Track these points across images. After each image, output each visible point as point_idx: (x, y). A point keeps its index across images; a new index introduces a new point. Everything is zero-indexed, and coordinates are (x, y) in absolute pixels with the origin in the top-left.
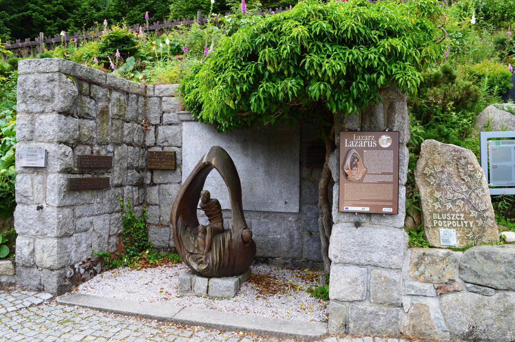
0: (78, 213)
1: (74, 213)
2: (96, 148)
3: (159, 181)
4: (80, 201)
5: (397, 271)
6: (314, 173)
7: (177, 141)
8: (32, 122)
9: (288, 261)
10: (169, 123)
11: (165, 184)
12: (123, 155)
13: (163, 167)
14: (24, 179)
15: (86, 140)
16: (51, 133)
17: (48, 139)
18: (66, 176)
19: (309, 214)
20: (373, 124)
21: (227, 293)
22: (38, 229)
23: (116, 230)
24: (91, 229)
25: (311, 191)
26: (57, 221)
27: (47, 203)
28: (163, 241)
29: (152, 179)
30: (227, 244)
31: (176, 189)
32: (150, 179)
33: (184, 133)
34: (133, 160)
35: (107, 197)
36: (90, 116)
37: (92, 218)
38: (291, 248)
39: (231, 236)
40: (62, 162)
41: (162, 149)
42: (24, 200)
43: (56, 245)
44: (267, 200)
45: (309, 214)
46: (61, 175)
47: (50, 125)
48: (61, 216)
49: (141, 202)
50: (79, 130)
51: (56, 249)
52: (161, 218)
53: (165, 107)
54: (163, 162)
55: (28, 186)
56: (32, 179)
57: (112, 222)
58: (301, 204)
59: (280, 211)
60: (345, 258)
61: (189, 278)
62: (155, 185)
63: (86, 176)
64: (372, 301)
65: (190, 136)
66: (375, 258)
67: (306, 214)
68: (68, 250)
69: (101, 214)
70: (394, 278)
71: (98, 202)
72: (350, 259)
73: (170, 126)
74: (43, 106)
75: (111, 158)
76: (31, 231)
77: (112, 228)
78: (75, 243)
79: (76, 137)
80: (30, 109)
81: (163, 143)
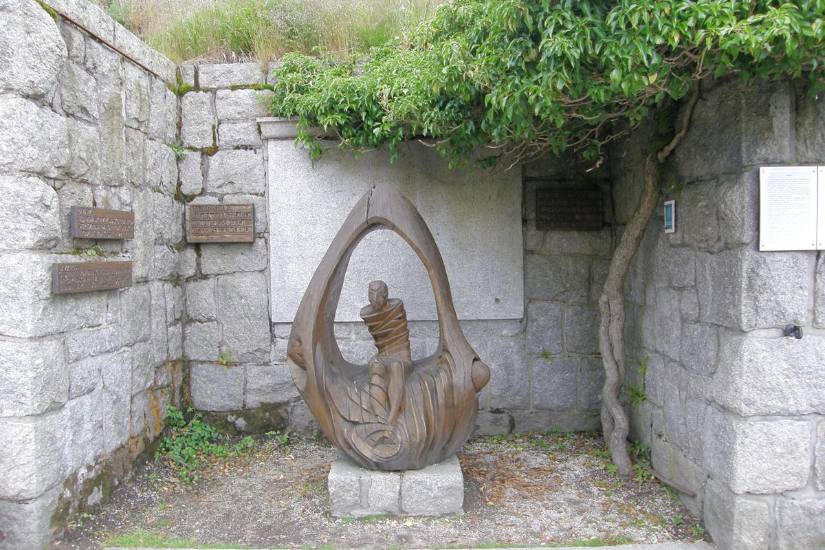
0: (74, 350)
1: (66, 351)
2: (101, 192)
3: (215, 269)
4: (75, 320)
7: (256, 181)
10: (235, 144)
11: (228, 274)
12: (154, 216)
13: (229, 237)
15: (83, 171)
18: (49, 259)
19: (542, 320)
21: (447, 501)
23: (142, 381)
24: (99, 387)
26: (31, 374)
29: (198, 264)
30: (441, 395)
32: (194, 265)
33: (271, 165)
34: (164, 224)
35: (125, 307)
36: (87, 113)
37: (99, 358)
38: (508, 389)
39: (450, 377)
40: (39, 222)
41: (221, 199)
43: (32, 436)
45: (542, 320)
46: (36, 257)
49: (177, 317)
50: (70, 147)
51: (31, 447)
52: (224, 348)
53: (224, 110)
54: (227, 227)
57: (136, 363)
58: (529, 300)
59: (486, 318)
60: (769, 403)
61: (355, 478)
62: (205, 277)
64: (821, 487)
65: (285, 170)
67: (536, 320)
68: (59, 444)
69: (117, 349)
71: (107, 319)
72: (780, 404)
73: (237, 151)
75: (131, 215)
77: (137, 378)
78: (69, 424)
79: (63, 162)
81: (220, 186)
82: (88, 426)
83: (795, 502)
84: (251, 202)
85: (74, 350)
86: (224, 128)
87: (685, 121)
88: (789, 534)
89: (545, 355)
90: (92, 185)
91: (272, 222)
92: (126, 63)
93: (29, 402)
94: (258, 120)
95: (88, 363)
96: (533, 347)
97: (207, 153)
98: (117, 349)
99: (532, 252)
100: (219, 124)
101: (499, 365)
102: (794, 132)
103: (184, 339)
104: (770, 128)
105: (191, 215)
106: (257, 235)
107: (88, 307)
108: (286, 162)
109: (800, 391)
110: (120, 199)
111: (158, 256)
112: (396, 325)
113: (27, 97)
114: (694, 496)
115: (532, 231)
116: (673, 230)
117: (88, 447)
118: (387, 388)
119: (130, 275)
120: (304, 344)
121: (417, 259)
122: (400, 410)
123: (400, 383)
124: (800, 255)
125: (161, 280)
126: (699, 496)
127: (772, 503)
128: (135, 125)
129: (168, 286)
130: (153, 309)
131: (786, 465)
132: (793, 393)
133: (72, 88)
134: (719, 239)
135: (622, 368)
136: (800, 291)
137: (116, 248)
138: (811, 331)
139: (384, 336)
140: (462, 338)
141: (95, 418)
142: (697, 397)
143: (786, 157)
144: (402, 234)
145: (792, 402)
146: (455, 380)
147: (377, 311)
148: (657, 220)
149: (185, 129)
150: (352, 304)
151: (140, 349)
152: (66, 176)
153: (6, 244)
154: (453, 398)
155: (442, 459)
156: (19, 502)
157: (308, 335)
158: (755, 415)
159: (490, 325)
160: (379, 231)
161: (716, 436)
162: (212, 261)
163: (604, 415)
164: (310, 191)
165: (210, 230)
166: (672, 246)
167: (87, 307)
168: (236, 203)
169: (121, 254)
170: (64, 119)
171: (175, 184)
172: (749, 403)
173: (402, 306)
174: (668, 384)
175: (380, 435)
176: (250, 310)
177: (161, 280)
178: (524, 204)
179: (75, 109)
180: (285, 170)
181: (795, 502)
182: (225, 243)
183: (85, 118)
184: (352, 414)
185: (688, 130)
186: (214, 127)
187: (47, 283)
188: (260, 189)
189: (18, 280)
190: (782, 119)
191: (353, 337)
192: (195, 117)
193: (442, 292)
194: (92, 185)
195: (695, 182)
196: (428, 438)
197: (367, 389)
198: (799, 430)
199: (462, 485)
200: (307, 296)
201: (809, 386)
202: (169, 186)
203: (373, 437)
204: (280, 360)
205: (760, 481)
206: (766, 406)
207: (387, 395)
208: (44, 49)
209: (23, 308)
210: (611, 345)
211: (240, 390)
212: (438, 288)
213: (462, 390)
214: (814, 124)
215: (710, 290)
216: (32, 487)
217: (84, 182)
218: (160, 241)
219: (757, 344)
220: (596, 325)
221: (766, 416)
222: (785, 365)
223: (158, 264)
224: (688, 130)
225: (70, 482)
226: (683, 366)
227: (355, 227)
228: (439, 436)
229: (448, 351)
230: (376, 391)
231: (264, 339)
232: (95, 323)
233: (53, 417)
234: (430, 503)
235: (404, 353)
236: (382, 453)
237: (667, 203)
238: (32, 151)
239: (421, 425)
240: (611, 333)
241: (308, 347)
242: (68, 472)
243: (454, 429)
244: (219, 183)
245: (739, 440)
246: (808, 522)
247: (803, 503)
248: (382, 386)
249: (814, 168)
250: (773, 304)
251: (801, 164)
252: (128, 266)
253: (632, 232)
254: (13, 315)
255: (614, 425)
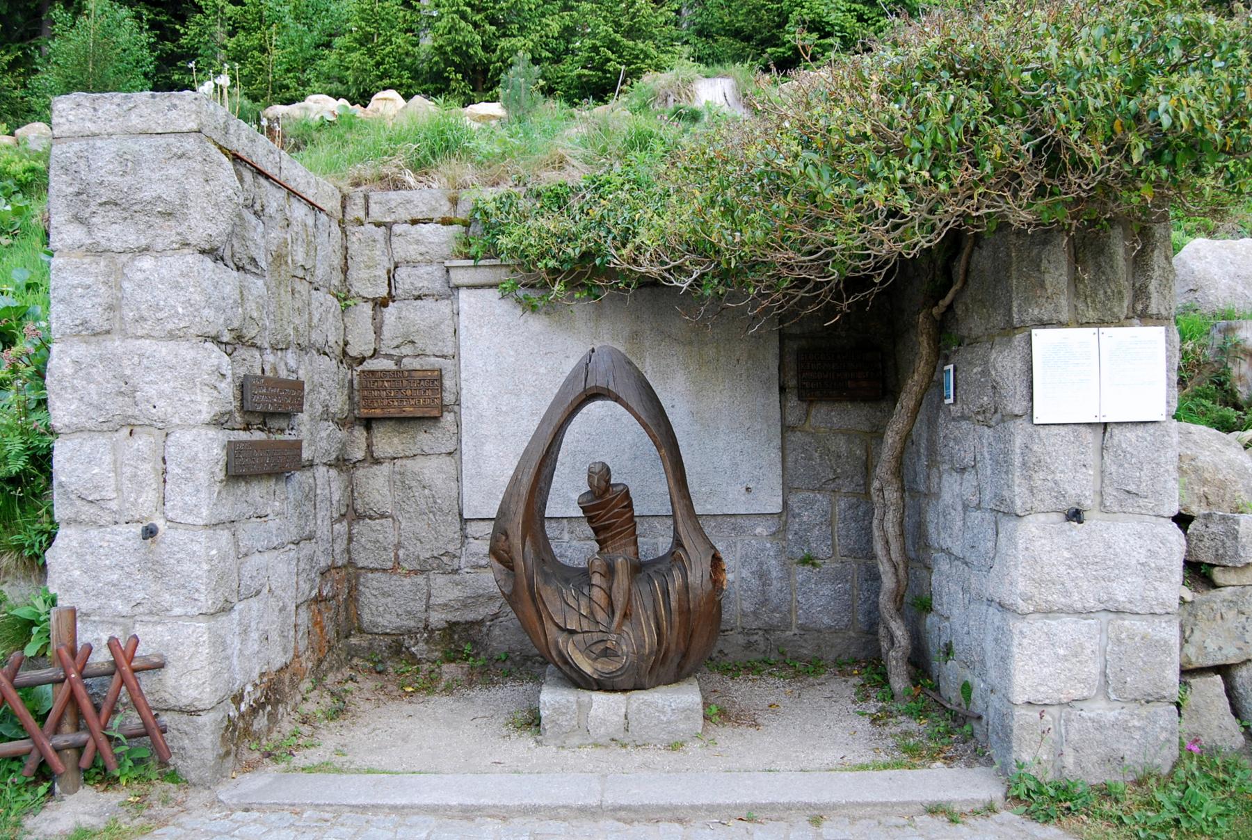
0: (244, 545)
2: (270, 358)
3: (390, 452)
5: (1167, 618)
6: (813, 412)
8: (115, 278)
9: (756, 637)
10: (416, 293)
11: (407, 457)
12: (325, 384)
13: (409, 411)
14: (87, 449)
15: (253, 333)
16: (180, 310)
17: (170, 326)
18: (224, 436)
20: (1103, 273)
22: (139, 596)
23: (308, 586)
24: (265, 590)
25: (811, 459)
26: (206, 567)
27: (170, 515)
28: (409, 613)
31: (441, 471)
32: (364, 446)
35: (291, 496)
36: (256, 265)
37: (266, 555)
38: (765, 602)
39: (685, 577)
42: (88, 511)
43: (205, 637)
44: (700, 486)
46: (212, 433)
47: (176, 286)
48: (214, 552)
51: (205, 650)
53: (402, 249)
55: (101, 470)
56: (114, 449)
58: (788, 489)
60: (1050, 598)
62: (377, 462)
63: (258, 436)
64: (1113, 697)
65: (481, 326)
66: (1121, 593)
69: (283, 545)
70: (1163, 635)
72: (1062, 599)
73: (419, 302)
74: (151, 232)
76: (113, 603)
79: (236, 324)
80: (103, 242)
81: (397, 347)
82: (255, 635)
83: (1083, 714)
84: (437, 366)
85: (244, 545)
86: (402, 273)
87: (961, 272)
88: (1076, 750)
89: (808, 561)
90: (260, 348)
91: (464, 392)
92: (292, 199)
93: (202, 599)
94: (447, 263)
95: (256, 559)
96: (795, 549)
97: (381, 304)
98: (283, 545)
99: (793, 429)
100: (396, 267)
101: (752, 573)
102: (1073, 289)
103: (350, 540)
104: (1042, 285)
105: (360, 383)
106: (443, 407)
107: (257, 493)
108: (481, 317)
109: (1085, 585)
110: (286, 364)
111: (324, 434)
112: (620, 515)
113: (203, 252)
114: (980, 718)
115: (793, 401)
116: (951, 400)
117: (255, 660)
118: (610, 589)
119: (300, 455)
120: (511, 538)
121: (647, 438)
122: (625, 616)
123: (626, 582)
124: (1082, 429)
125: (325, 464)
126: (985, 717)
127: (1057, 716)
128: (301, 273)
129: (333, 473)
130: (319, 499)
131: (1070, 670)
132: (1077, 586)
133: (243, 238)
134: (996, 412)
135: (901, 572)
136: (1084, 470)
137: (284, 424)
138: (1100, 515)
139: (606, 528)
140: (700, 530)
141: (261, 626)
142: (979, 598)
143: (1064, 317)
144: (627, 407)
145: (1076, 597)
146: (690, 579)
147: (597, 498)
148: (934, 384)
149: (353, 273)
150: (566, 496)
151: (307, 548)
152: (236, 342)
153: (181, 419)
154: (688, 601)
155: (679, 676)
156: (190, 713)
157: (516, 527)
158: (1034, 612)
159: (739, 520)
160: (599, 403)
161: (996, 640)
162: (387, 442)
163: (882, 631)
164: (512, 353)
165: (385, 402)
166: (954, 419)
167: (258, 492)
168: (418, 367)
169: (287, 432)
170: (235, 273)
171: (341, 344)
172: (1027, 598)
173: (628, 492)
174: (953, 588)
175: (601, 646)
176: (435, 502)
177: (325, 464)
178: (781, 369)
179: (245, 261)
180: (481, 326)
181: (1083, 714)
182: (405, 419)
183: (254, 270)
184: (568, 621)
185: (965, 282)
186: (389, 272)
187: (222, 463)
188: (449, 351)
189: (193, 459)
190: (1057, 272)
191: (566, 537)
192: (366, 259)
193: (674, 475)
194: (260, 348)
195: (975, 341)
196: (659, 650)
197: (586, 591)
198: (1084, 630)
199: (700, 706)
200: (515, 481)
201: (1096, 578)
202: (334, 346)
203: (593, 648)
204: (472, 567)
205: (1042, 689)
206: (1046, 602)
207: (609, 597)
208: (222, 199)
209: (198, 491)
210: (887, 542)
211: (421, 606)
212: (670, 470)
213: (699, 592)
214: (1096, 279)
215: (989, 472)
216: (205, 696)
217: (254, 345)
218: (326, 415)
219: (1033, 529)
220: (870, 513)
221: (1048, 612)
222: (1066, 554)
223: (324, 444)
224: (965, 282)
225: (238, 699)
226: (966, 563)
227: (571, 398)
228: (673, 646)
229: (682, 546)
230: (597, 594)
231: (453, 540)
232: (263, 513)
233: (223, 618)
234: (663, 729)
235: (631, 549)
236: (609, 666)
237: (946, 368)
238: (208, 313)
239: (650, 632)
240: (887, 524)
241: (516, 541)
242: (236, 687)
243: (690, 641)
244: (395, 343)
245: (1016, 642)
246: (1098, 736)
247: (1092, 715)
248: (604, 586)
249: (1095, 330)
250: (1050, 484)
251: (1081, 325)
252: (297, 445)
253: (907, 401)
254: (187, 499)
255: (893, 644)
